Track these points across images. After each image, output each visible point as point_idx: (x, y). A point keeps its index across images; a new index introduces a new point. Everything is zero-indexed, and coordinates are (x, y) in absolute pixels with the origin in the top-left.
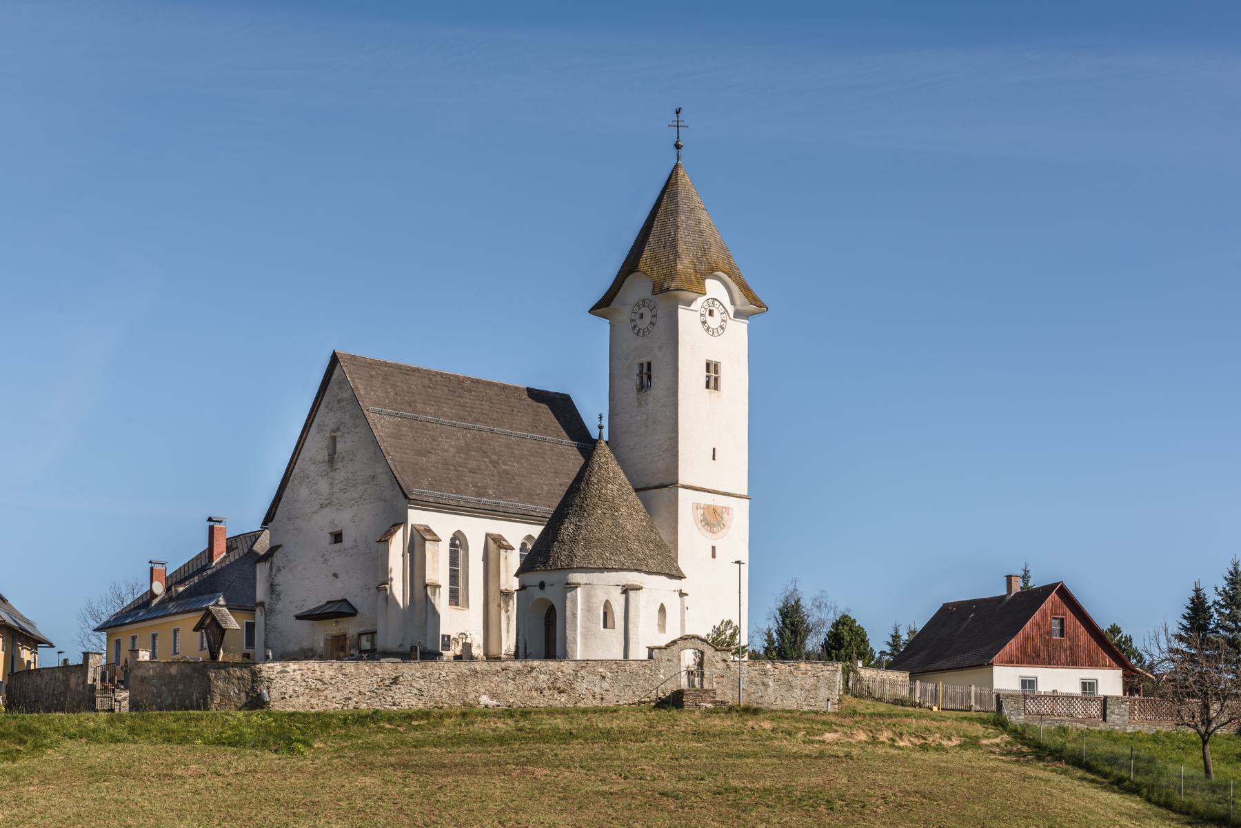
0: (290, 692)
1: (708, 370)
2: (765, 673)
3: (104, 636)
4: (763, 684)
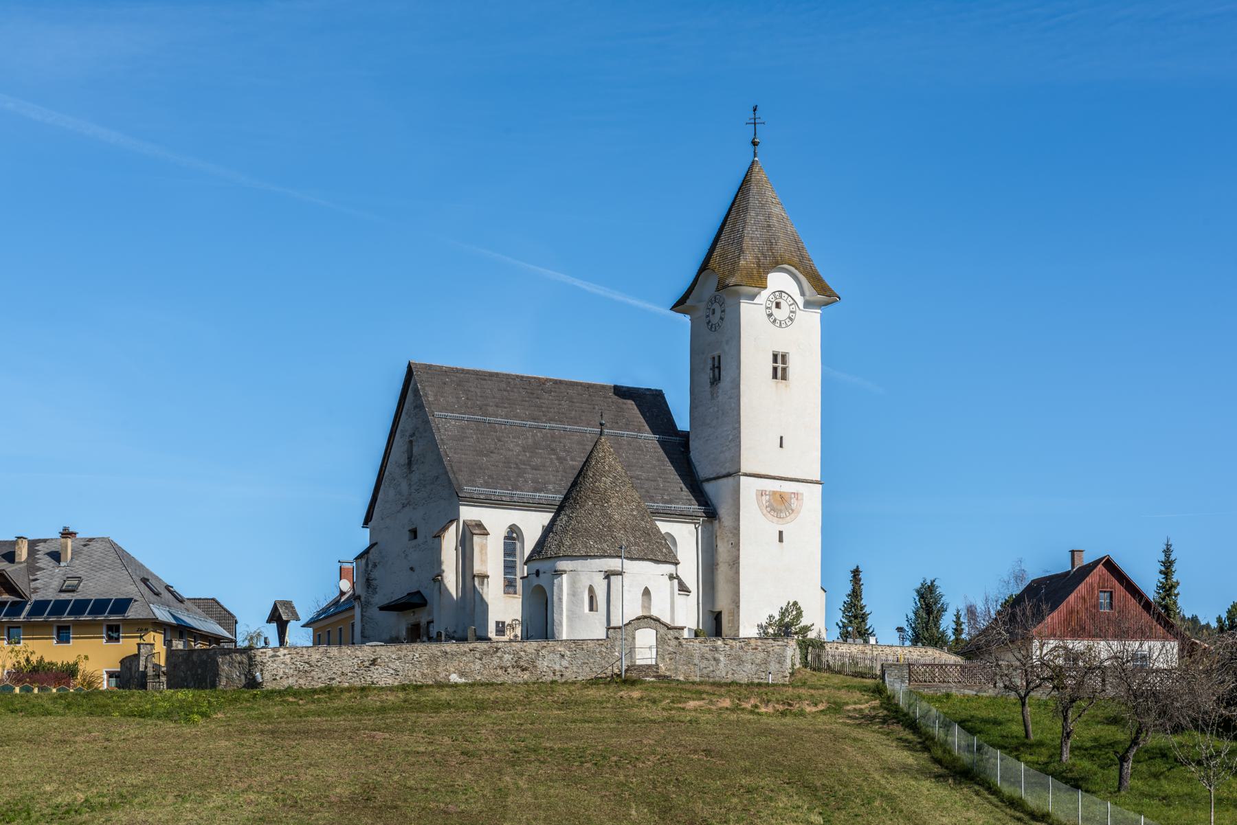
0: (281, 674)
1: (775, 361)
2: (716, 649)
4: (714, 659)
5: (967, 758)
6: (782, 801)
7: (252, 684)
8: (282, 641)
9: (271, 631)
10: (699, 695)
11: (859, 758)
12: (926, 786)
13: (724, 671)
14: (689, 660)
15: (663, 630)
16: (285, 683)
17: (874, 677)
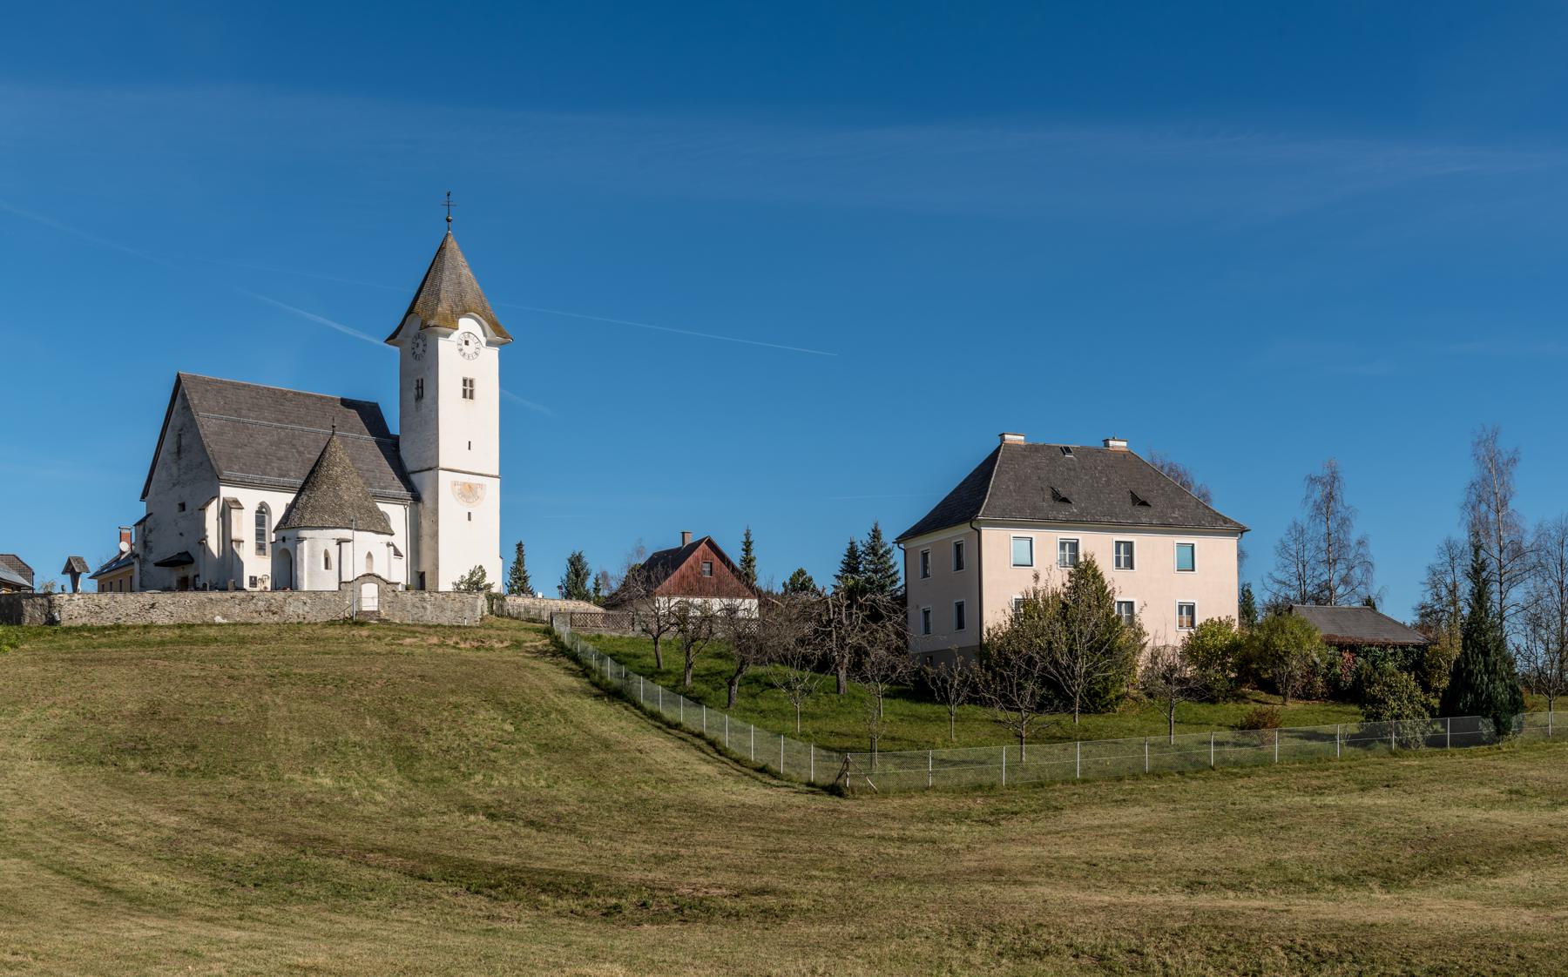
2: (424, 600)
3: (95, 581)
5: (616, 682)
6: (482, 714)
7: (52, 621)
8: (75, 590)
9: (66, 580)
10: (413, 634)
11: (537, 682)
12: (588, 703)
13: (430, 616)
14: (403, 607)
15: (383, 585)
16: (80, 622)
17: (542, 622)
